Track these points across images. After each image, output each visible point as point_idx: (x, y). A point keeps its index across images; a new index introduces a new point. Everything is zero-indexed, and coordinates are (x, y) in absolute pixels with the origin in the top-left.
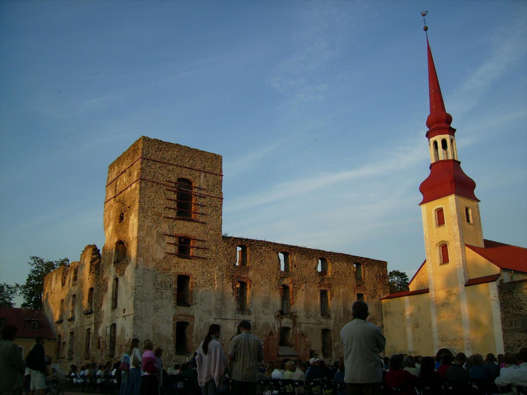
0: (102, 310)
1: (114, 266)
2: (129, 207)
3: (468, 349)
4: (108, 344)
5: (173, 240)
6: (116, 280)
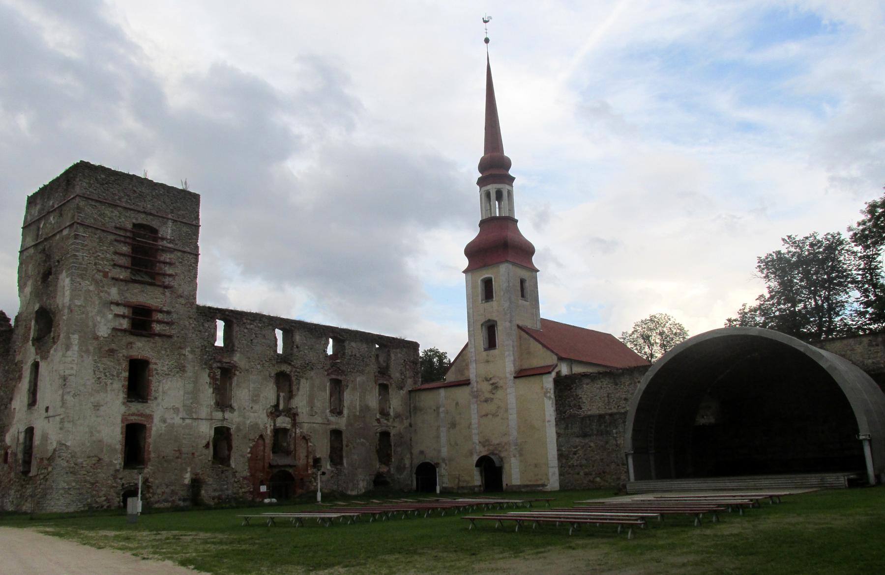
0: (13, 407)
1: (33, 345)
2: (58, 261)
3: (515, 456)
4: (20, 456)
5: (121, 310)
6: (36, 366)
